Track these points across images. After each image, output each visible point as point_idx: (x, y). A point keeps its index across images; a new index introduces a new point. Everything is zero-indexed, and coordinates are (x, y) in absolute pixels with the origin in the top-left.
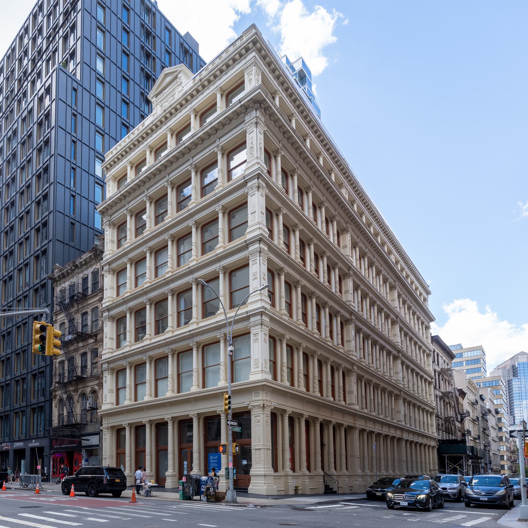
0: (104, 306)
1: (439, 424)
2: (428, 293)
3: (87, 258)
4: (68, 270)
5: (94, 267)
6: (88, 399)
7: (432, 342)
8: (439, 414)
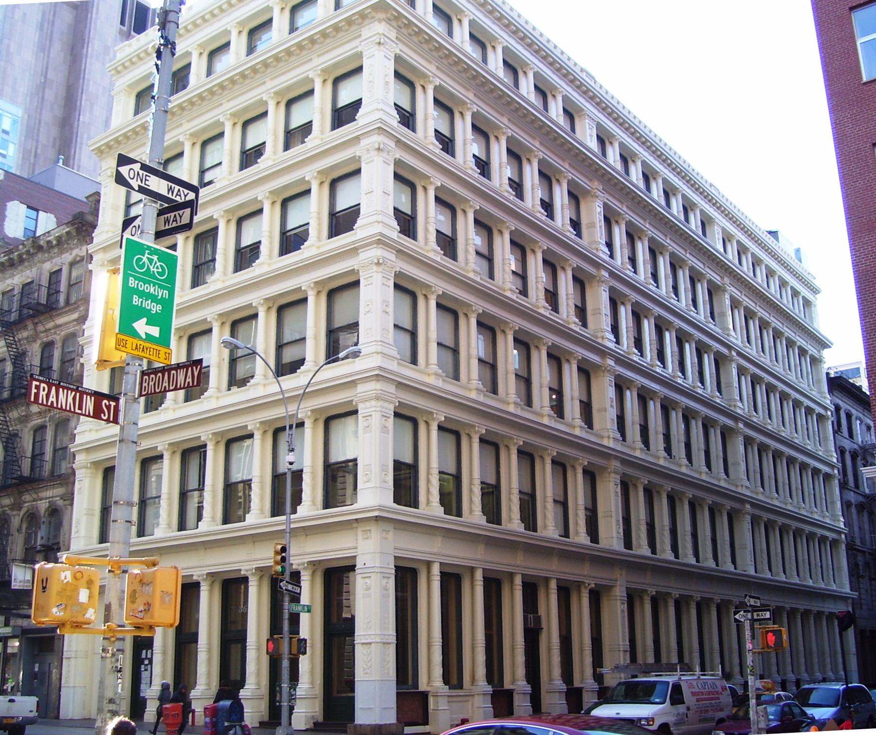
1: (857, 565)
2: (815, 291)
4: (23, 254)
6: (40, 528)
7: (830, 391)
8: (858, 542)
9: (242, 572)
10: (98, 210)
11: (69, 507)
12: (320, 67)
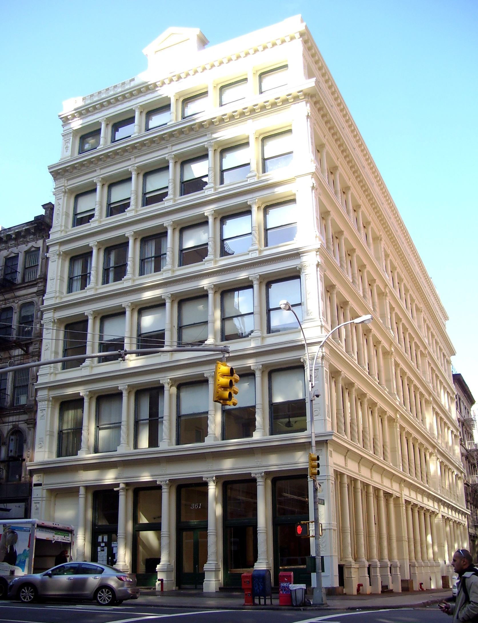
0: (46, 303)
3: (21, 231)
5: (30, 245)
9: (158, 483)
10: (52, 216)
11: (32, 429)
12: (101, 176)
